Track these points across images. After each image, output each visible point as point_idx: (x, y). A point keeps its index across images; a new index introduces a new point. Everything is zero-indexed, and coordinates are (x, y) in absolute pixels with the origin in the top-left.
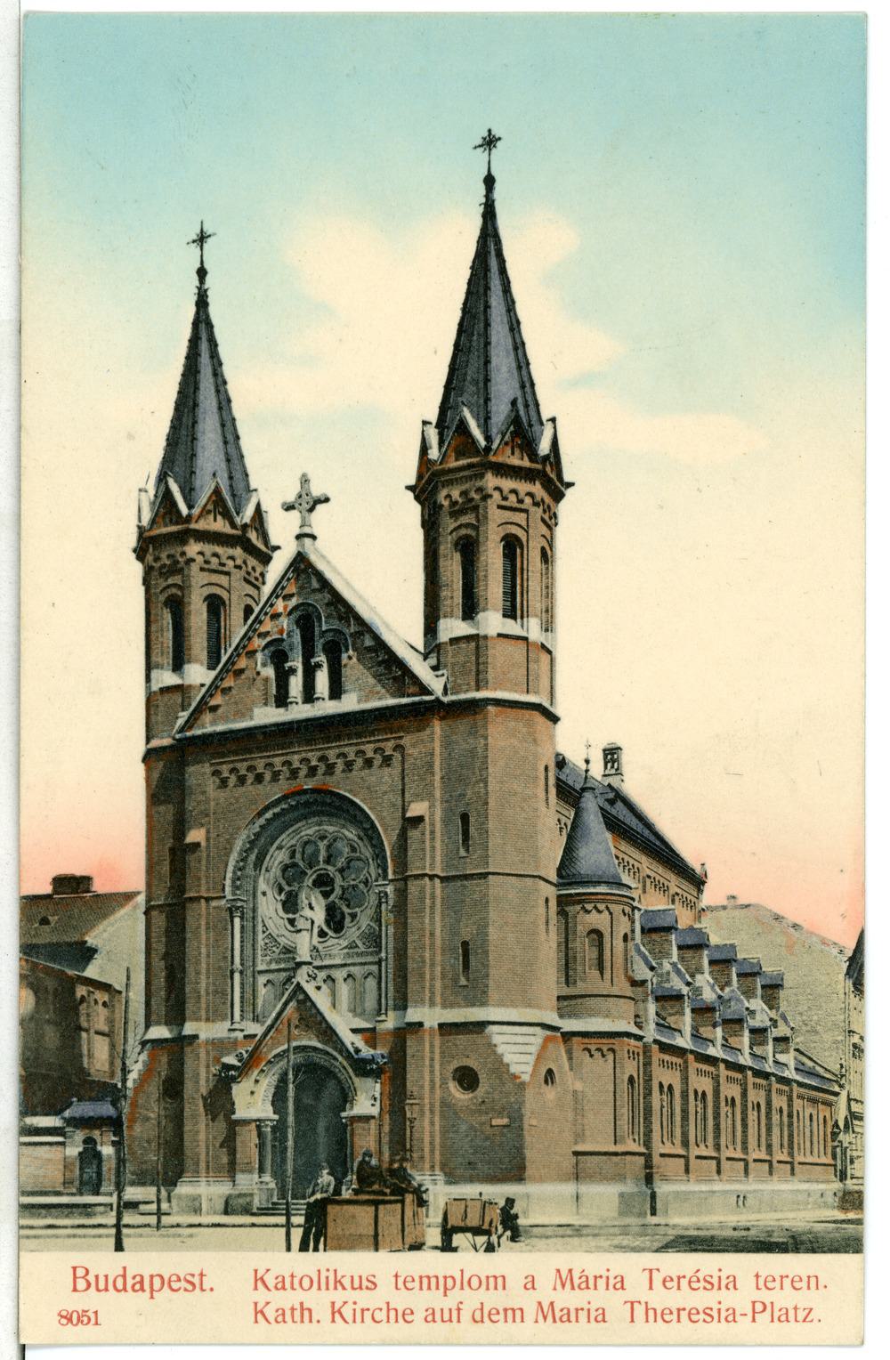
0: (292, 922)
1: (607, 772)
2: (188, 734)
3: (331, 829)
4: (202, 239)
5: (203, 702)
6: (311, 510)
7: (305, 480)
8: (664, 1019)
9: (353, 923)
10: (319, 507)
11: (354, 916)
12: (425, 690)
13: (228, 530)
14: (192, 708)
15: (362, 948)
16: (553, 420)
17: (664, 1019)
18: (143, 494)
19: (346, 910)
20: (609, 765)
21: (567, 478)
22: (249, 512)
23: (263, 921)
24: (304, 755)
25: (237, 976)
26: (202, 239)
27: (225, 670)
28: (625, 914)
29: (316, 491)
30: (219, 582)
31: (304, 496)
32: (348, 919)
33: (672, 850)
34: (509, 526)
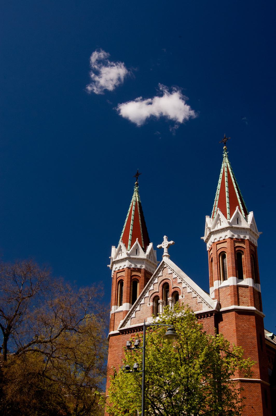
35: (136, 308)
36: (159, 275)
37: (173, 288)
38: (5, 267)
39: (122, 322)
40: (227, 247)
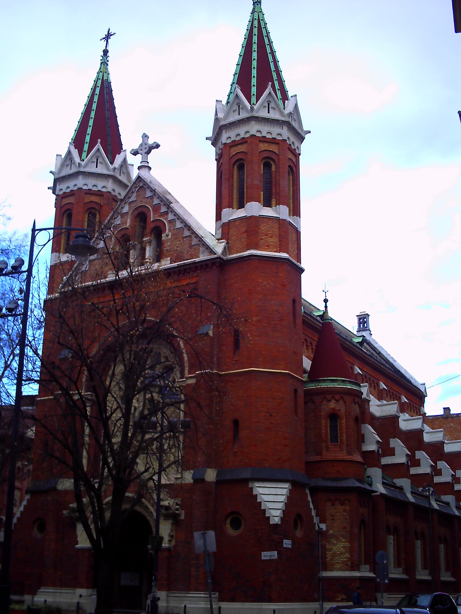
4: (108, 37)
6: (148, 152)
7: (145, 136)
12: (212, 252)
13: (105, 172)
21: (305, 128)
26: (108, 37)
28: (355, 403)
29: (151, 142)
31: (144, 144)
33: (379, 353)
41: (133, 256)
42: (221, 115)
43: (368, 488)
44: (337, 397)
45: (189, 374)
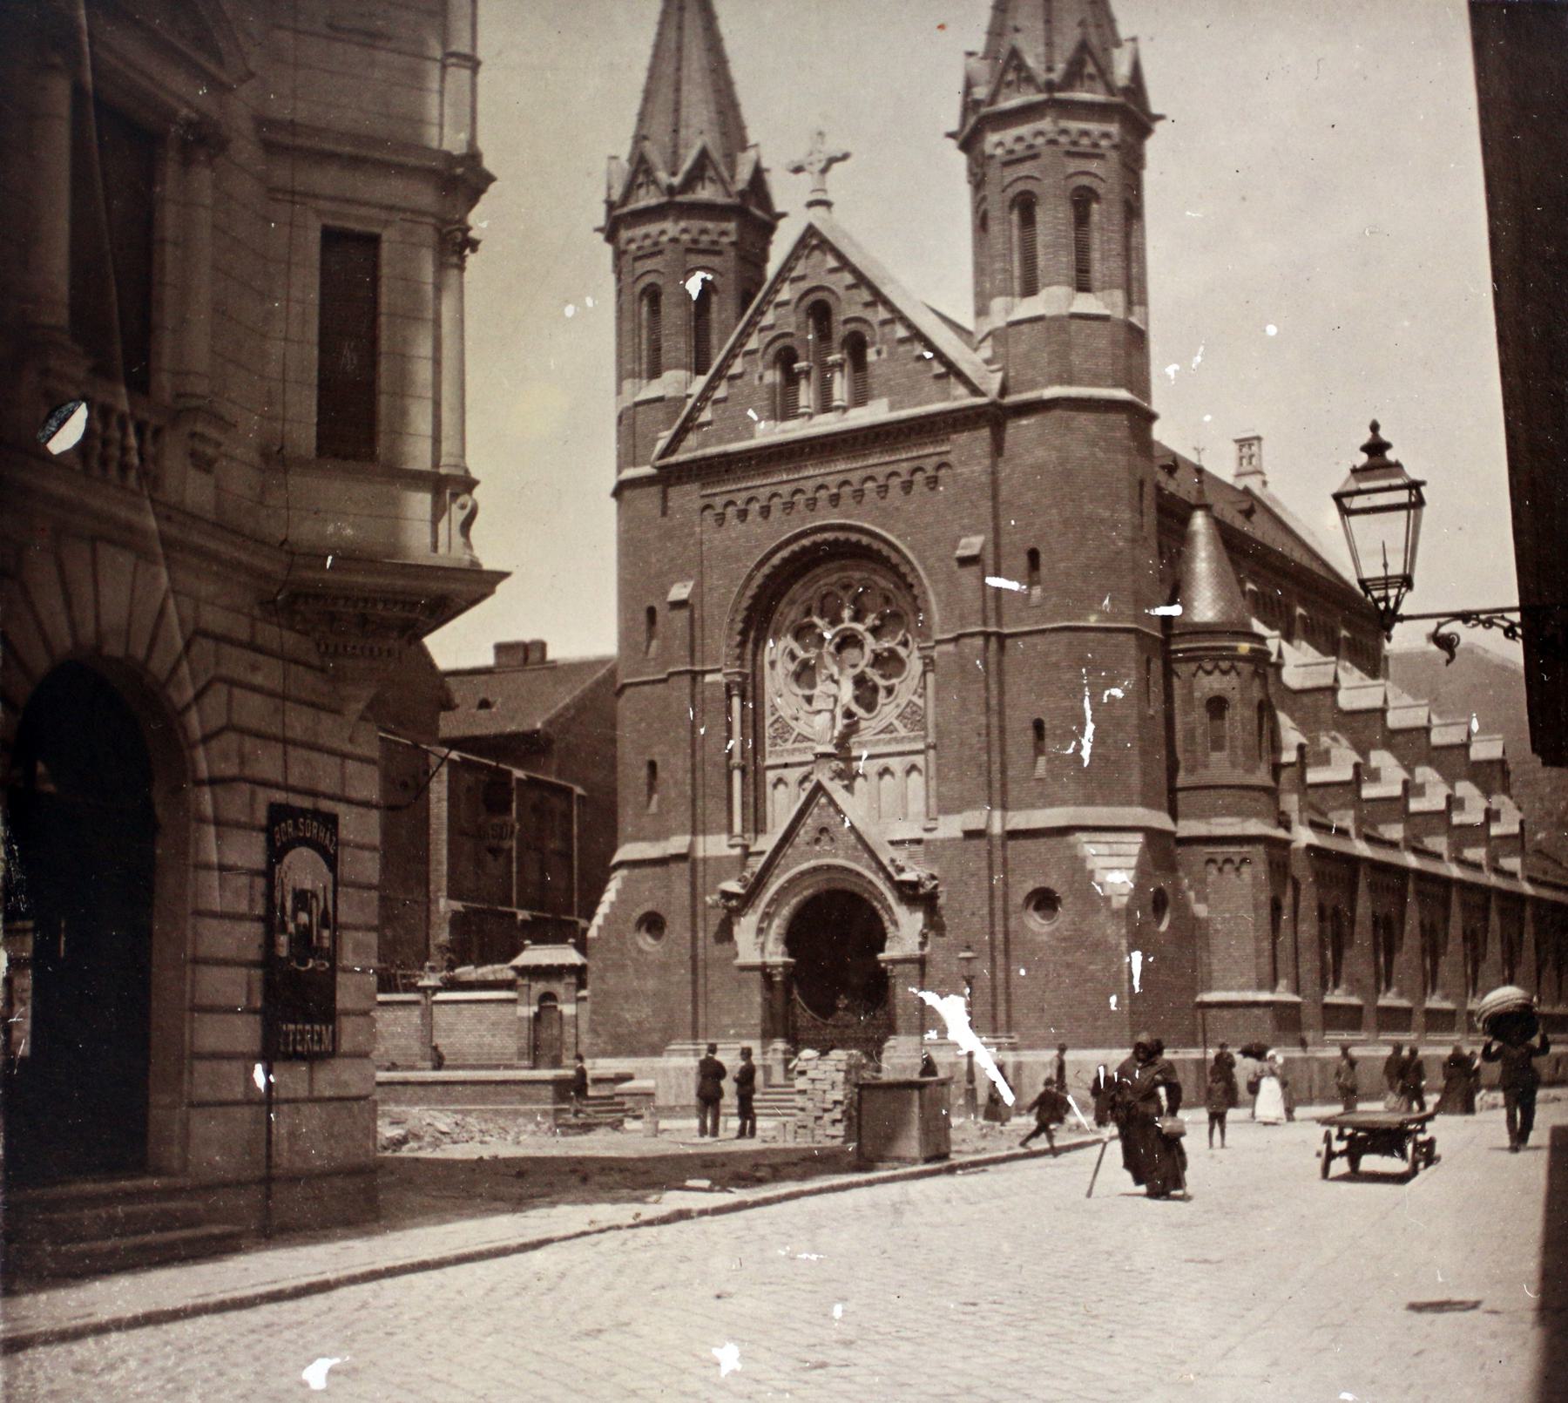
0: (809, 700)
1: (1243, 470)
2: (673, 459)
3: (857, 575)
5: (690, 418)
6: (824, 171)
8: (1324, 814)
9: (891, 699)
10: (836, 167)
11: (890, 691)
12: (975, 391)
13: (721, 199)
14: (711, 371)
15: (903, 732)
16: (1134, 40)
17: (1324, 814)
18: (614, 163)
19: (881, 682)
20: (1245, 462)
22: (744, 174)
23: (357, 1310)
24: (820, 481)
25: (737, 775)
27: (719, 375)
30: (710, 265)
32: (882, 693)
34: (1075, 179)
35: (777, 291)
36: (794, 274)
37: (846, 322)
38: (1473, 1047)
39: (665, 437)
40: (1036, 175)
41: (806, 395)
42: (981, 92)
43: (776, 237)
44: (1224, 665)
45: (943, 632)
